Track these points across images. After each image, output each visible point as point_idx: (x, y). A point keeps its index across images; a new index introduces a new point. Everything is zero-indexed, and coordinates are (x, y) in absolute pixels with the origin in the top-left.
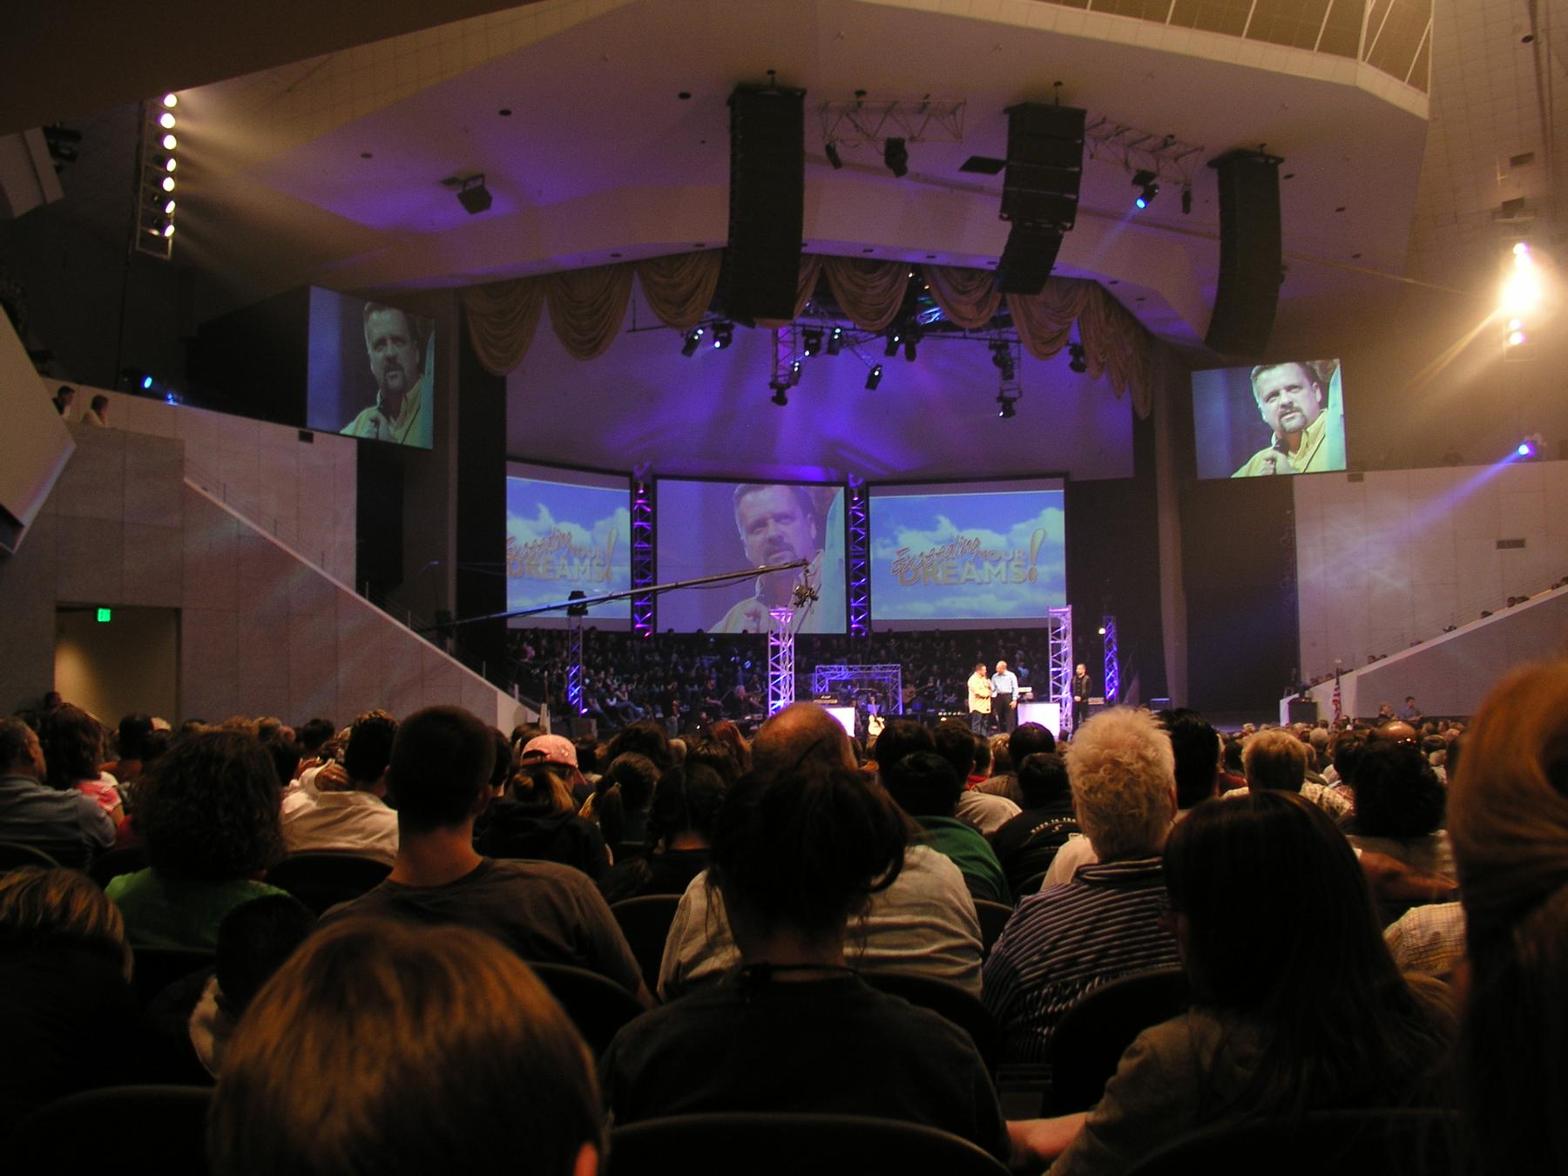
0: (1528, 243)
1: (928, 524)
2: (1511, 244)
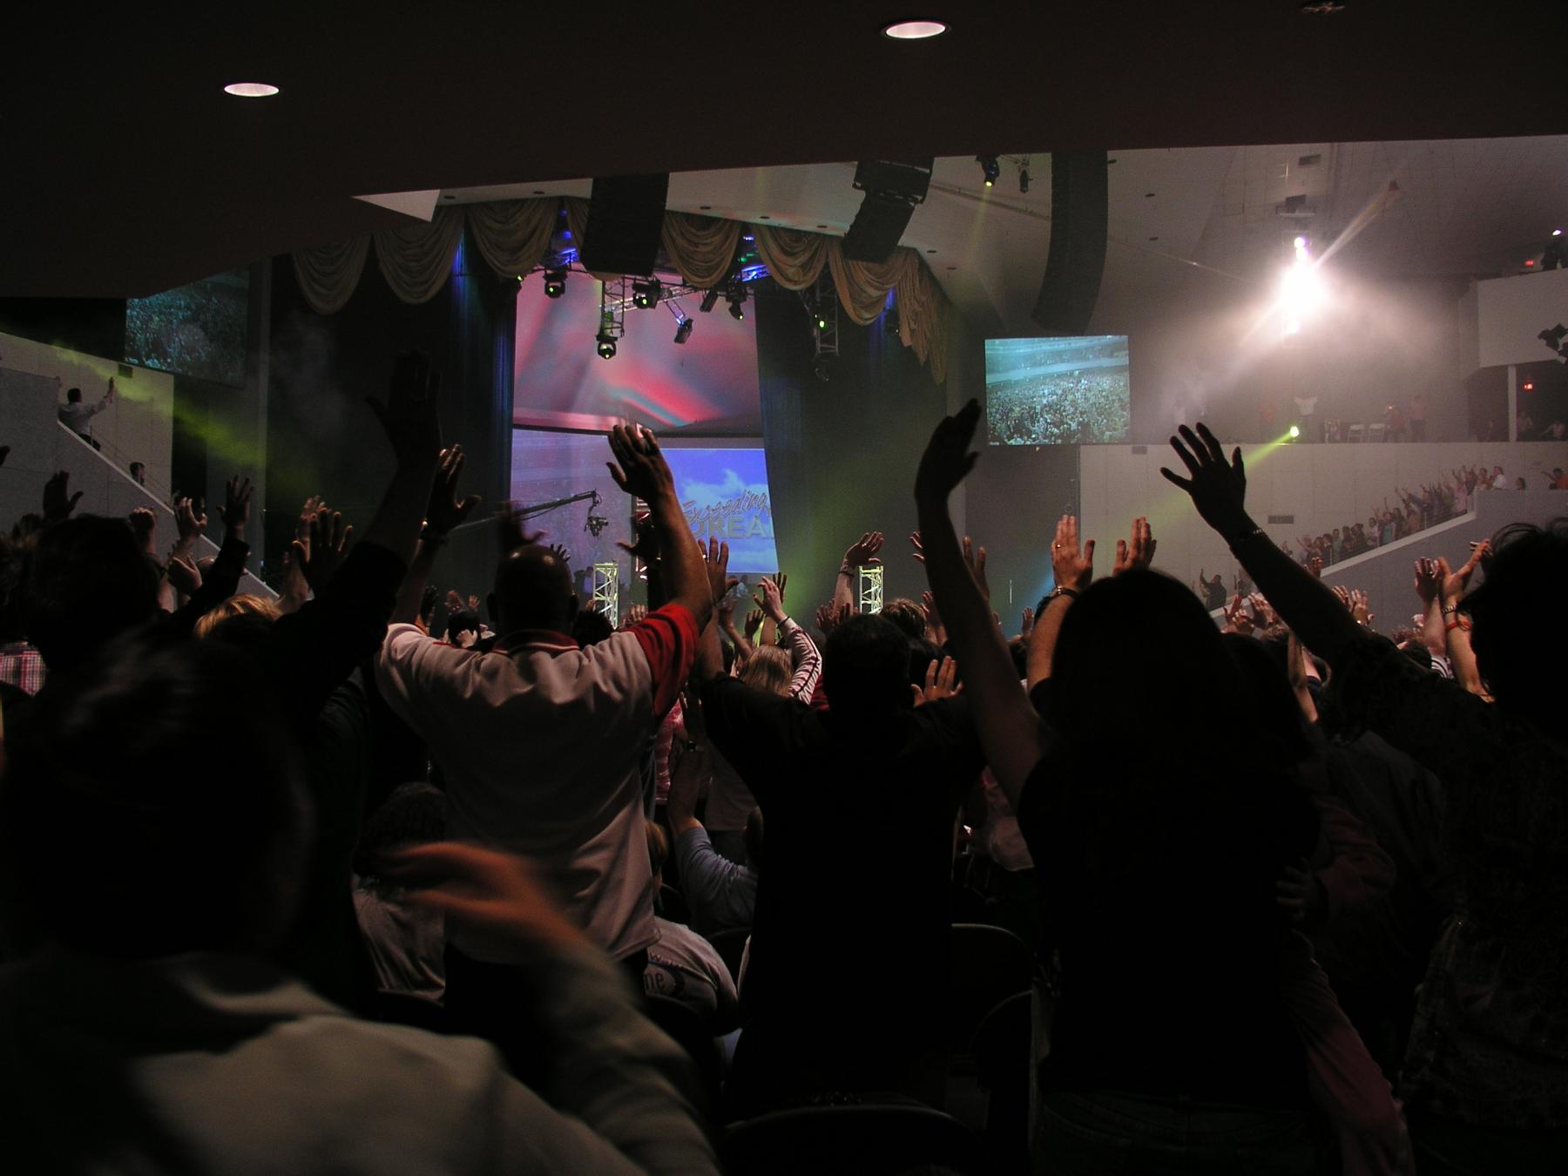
0: (1307, 237)
1: (716, 478)
2: (1292, 238)
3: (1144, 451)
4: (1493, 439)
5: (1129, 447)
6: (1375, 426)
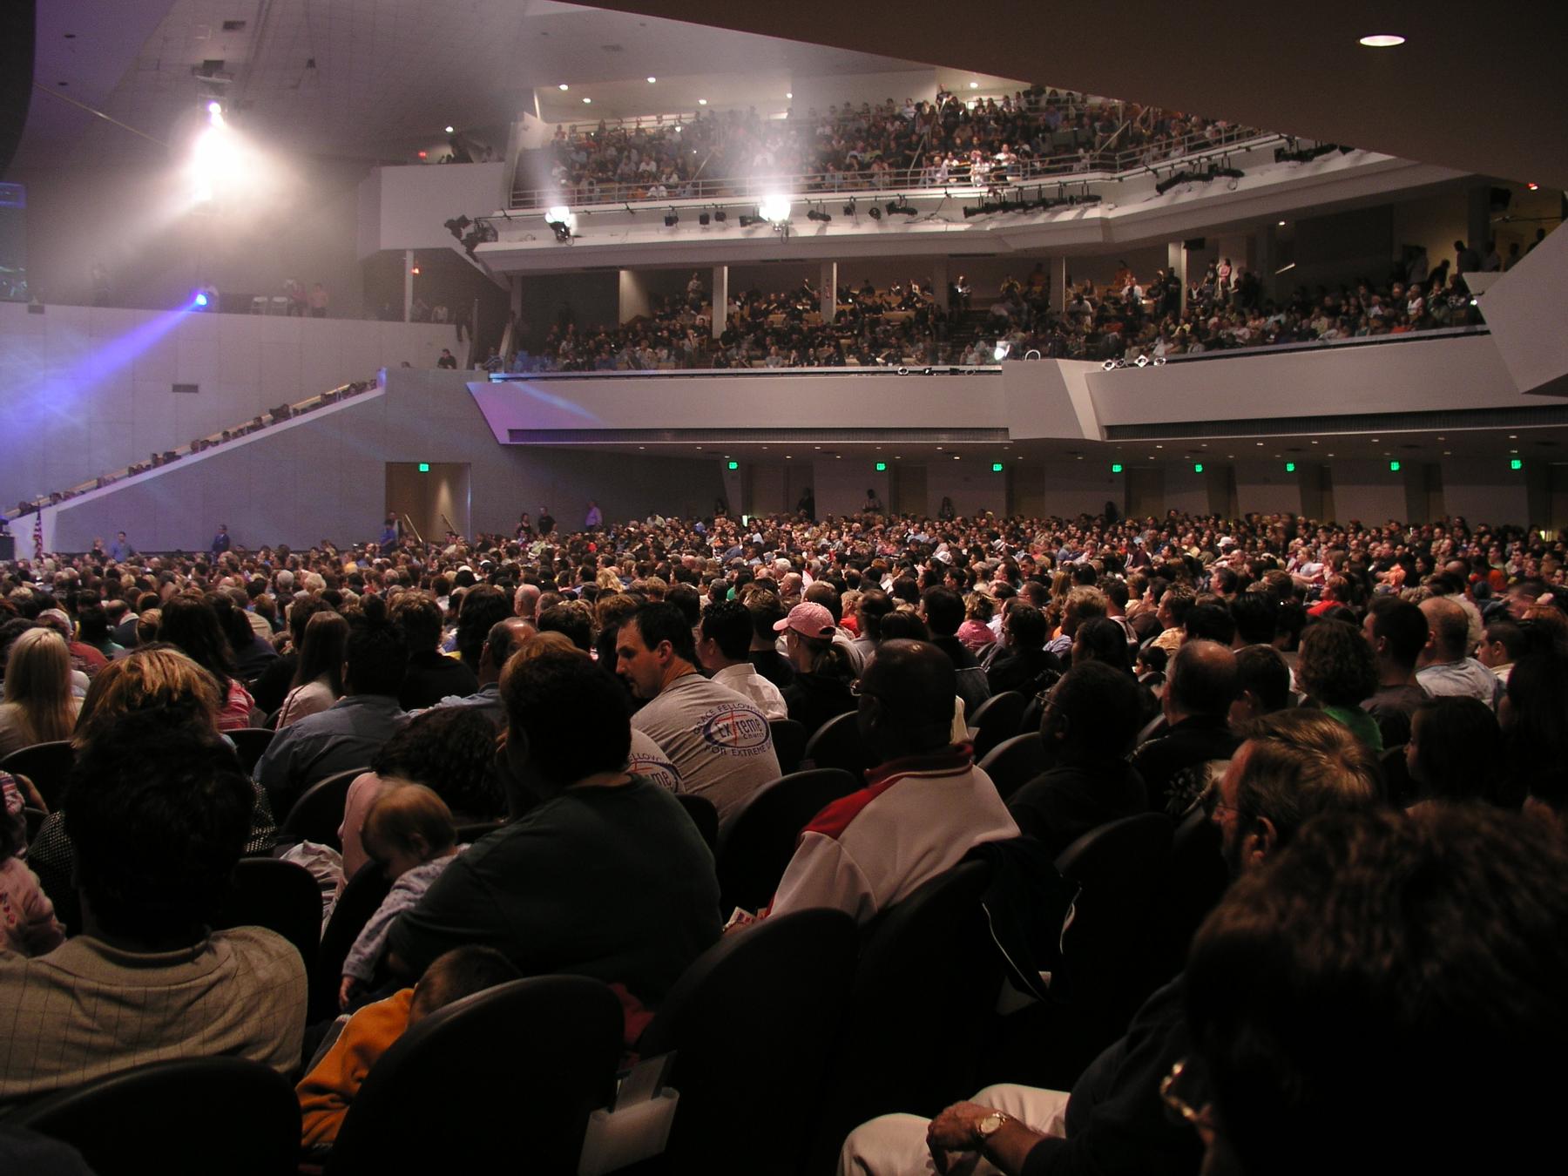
3: (40, 310)
4: (384, 316)
5: (25, 306)
6: (277, 299)
